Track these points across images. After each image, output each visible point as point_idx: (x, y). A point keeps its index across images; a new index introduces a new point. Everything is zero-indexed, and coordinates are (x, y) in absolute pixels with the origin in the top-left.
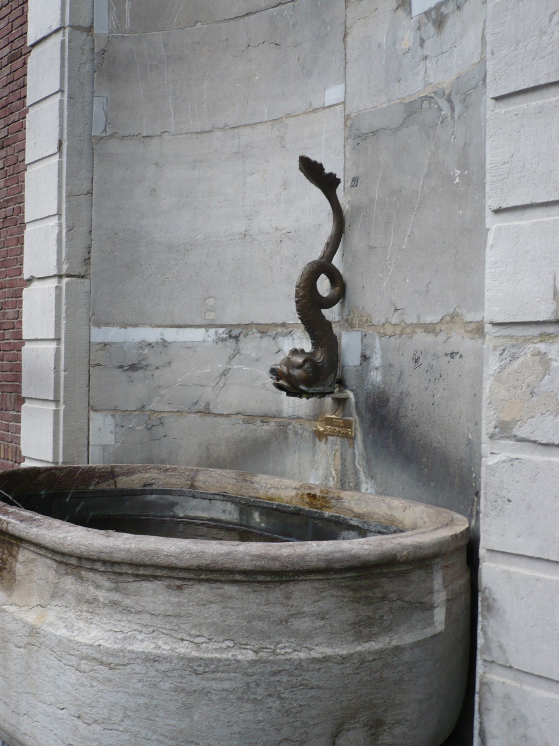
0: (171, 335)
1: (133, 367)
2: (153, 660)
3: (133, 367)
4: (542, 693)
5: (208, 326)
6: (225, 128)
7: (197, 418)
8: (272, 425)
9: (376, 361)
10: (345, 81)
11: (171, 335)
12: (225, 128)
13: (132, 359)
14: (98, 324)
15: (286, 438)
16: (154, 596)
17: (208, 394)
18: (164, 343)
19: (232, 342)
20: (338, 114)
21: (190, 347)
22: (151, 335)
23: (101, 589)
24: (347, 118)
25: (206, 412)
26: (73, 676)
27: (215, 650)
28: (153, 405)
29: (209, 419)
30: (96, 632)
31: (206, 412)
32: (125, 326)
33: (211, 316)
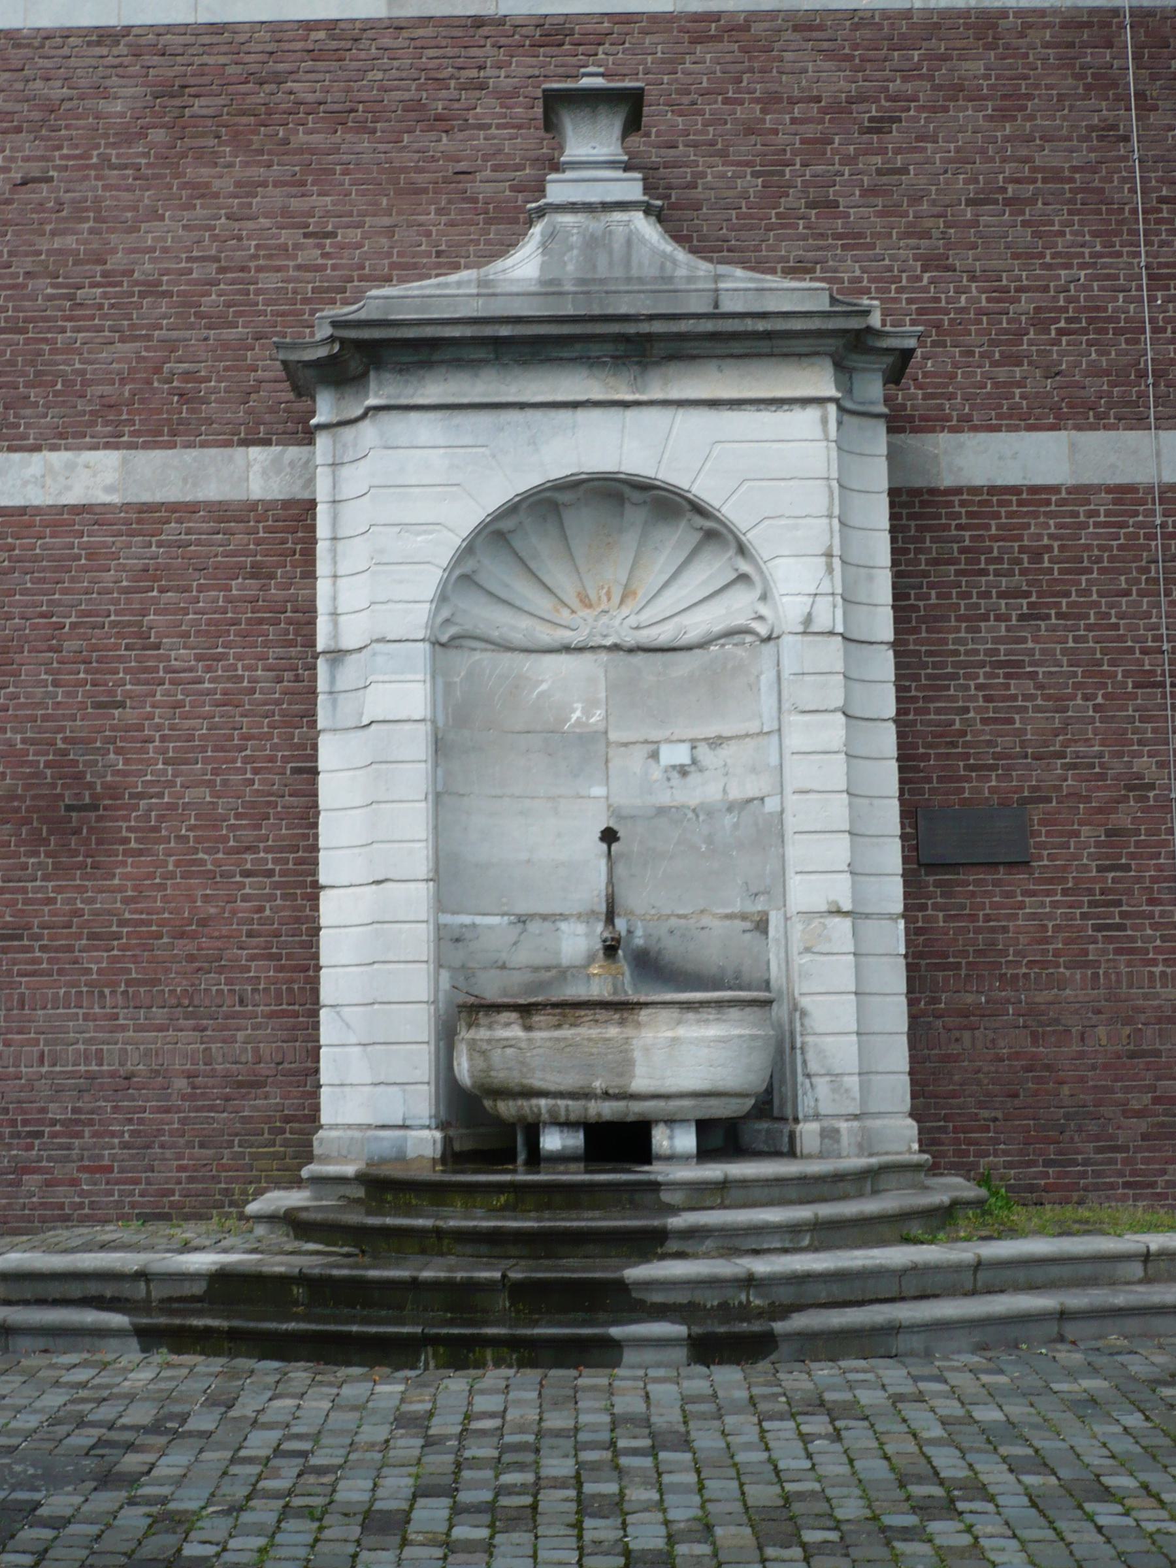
0: (479, 920)
1: (457, 940)
2: (740, 1036)
3: (457, 940)
4: (829, 1039)
5: (503, 915)
6: (512, 796)
7: (498, 972)
8: (554, 972)
9: (639, 932)
10: (607, 784)
11: (479, 920)
12: (512, 796)
13: (456, 935)
14: (443, 912)
15: (565, 979)
16: (734, 1013)
17: (504, 956)
18: (474, 925)
19: (520, 925)
20: (602, 805)
21: (490, 927)
22: (466, 919)
23: (712, 1014)
24: (609, 806)
25: (503, 967)
26: (706, 1050)
27: (755, 1032)
28: (471, 965)
29: (505, 972)
30: (713, 1031)
31: (503, 967)
32: (453, 913)
33: (505, 909)
